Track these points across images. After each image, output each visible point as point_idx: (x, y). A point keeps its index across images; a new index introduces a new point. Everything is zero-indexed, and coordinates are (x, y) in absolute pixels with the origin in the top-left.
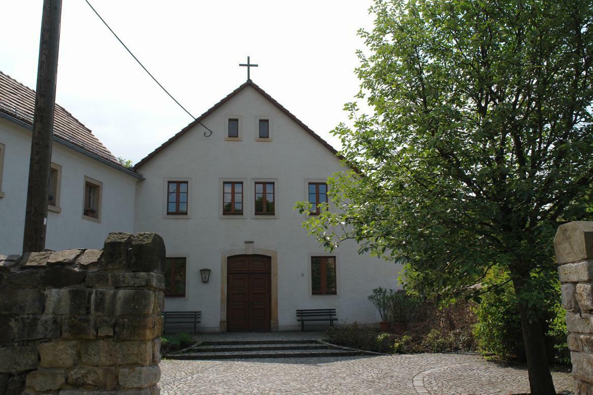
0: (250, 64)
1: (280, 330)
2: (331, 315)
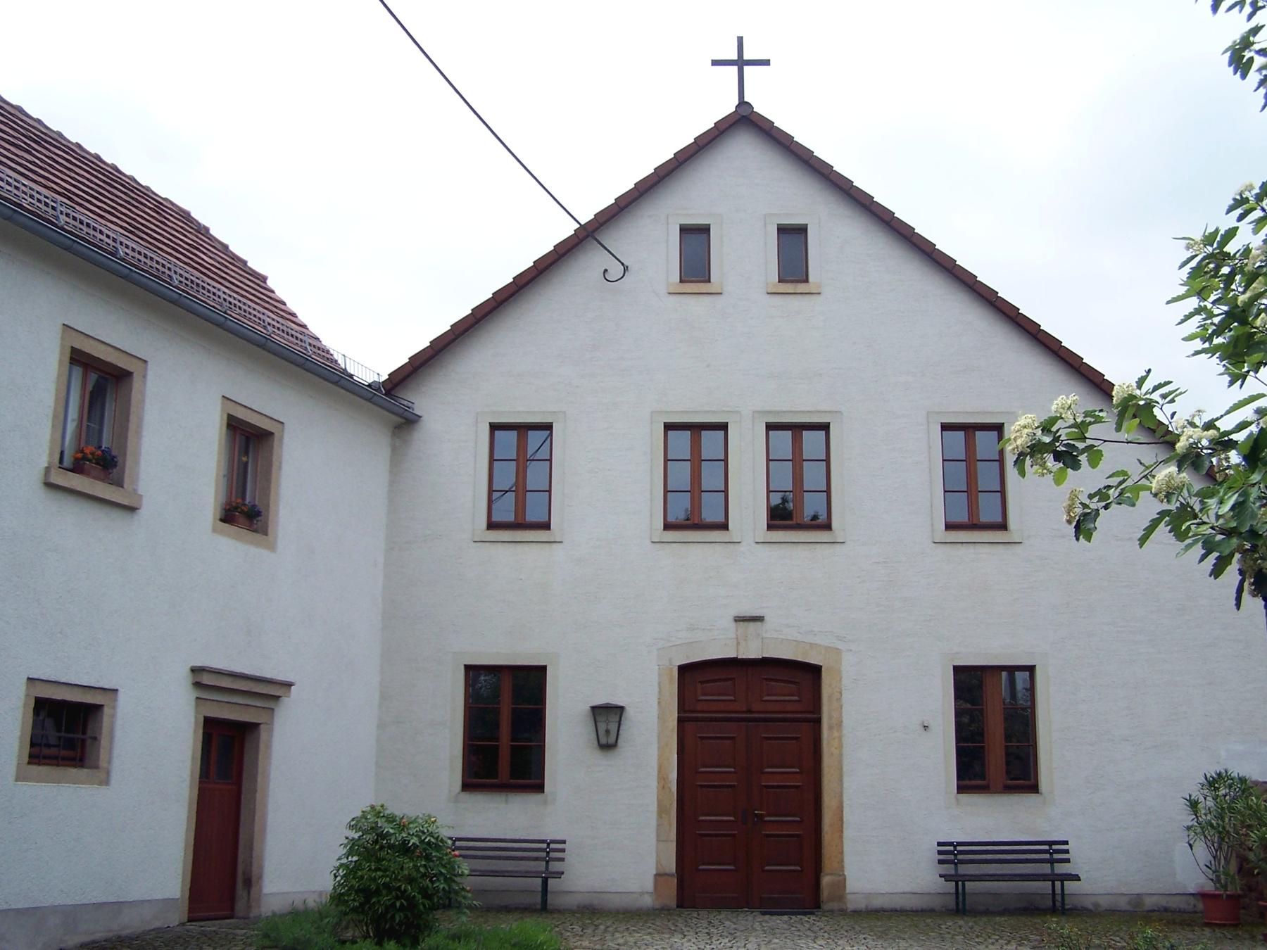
0: (746, 57)
1: (851, 906)
2: (1052, 862)
